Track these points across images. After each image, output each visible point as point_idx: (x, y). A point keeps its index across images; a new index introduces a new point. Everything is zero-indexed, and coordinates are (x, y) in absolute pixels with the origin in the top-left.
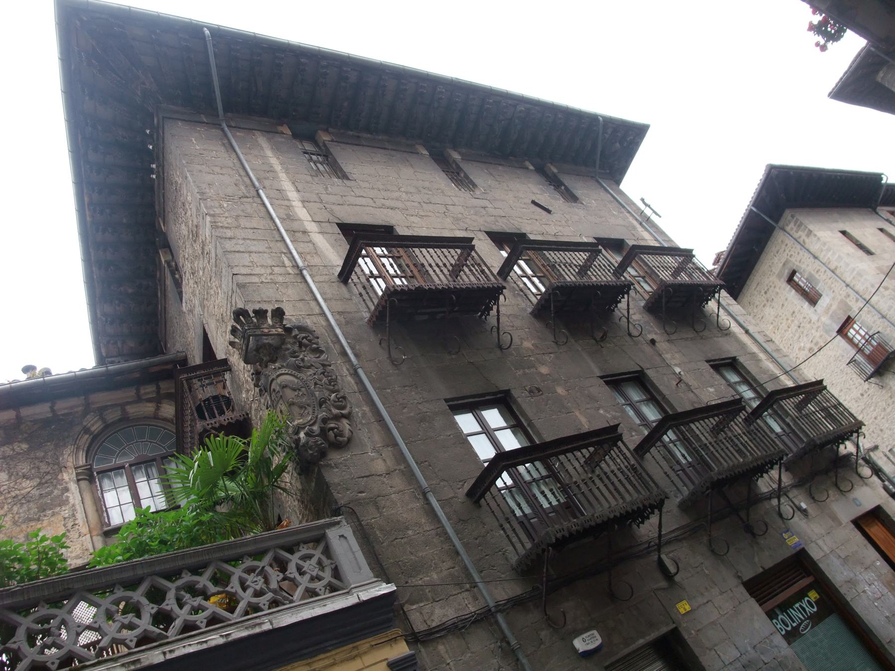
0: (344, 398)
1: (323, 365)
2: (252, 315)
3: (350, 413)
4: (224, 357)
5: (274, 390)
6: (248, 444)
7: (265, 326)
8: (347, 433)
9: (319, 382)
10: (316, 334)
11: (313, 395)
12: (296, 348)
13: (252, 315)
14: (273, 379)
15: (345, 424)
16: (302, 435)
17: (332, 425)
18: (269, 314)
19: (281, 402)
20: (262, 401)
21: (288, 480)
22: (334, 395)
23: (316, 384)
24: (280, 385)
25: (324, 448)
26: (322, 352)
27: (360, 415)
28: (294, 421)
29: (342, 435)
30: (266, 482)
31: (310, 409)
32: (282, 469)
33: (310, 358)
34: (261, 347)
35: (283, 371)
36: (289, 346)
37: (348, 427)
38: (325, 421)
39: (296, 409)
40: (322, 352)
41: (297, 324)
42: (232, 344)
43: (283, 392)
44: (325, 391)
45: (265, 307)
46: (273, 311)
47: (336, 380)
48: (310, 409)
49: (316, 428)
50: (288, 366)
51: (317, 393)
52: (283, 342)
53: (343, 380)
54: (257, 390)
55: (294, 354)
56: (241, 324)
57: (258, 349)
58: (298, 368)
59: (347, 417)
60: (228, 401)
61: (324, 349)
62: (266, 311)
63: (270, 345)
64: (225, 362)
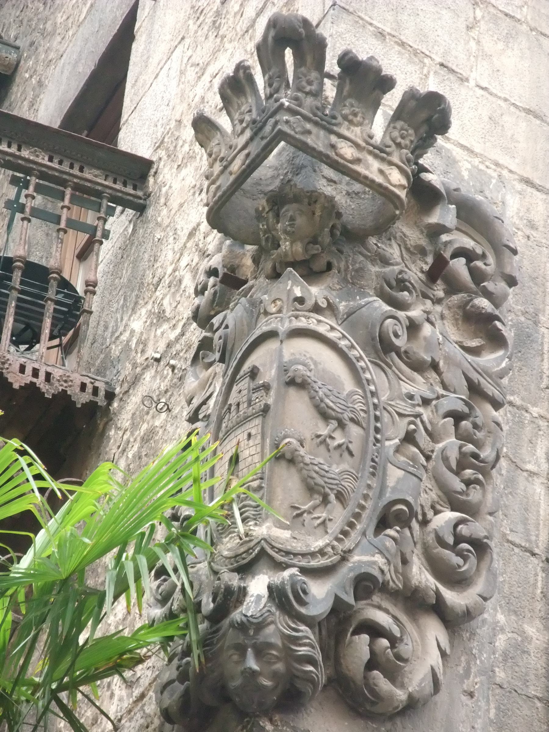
0: (480, 547)
1: (475, 389)
2: (332, 65)
3: (469, 615)
4: (144, 151)
5: (254, 373)
6: (54, 502)
7: (355, 133)
8: (417, 679)
9: (423, 438)
10: (514, 264)
11: (377, 470)
12: (415, 273)
13: (332, 65)
14: (272, 335)
15: (427, 643)
16: (258, 585)
17: (382, 618)
18: (391, 100)
19: (254, 427)
20: (191, 383)
21: (112, 710)
22: (449, 516)
23: (409, 438)
24: (284, 369)
25: (309, 679)
26: (497, 340)
27: (501, 641)
28: (258, 518)
29: (393, 675)
30: (37, 669)
31: (338, 515)
32: (119, 659)
33: (442, 334)
34: (296, 199)
35: (323, 325)
36: (394, 251)
37: (434, 658)
38: (366, 585)
39: (288, 486)
40: (497, 340)
41: (469, 190)
42: (203, 126)
43: (281, 398)
44: (427, 483)
45: (391, 63)
46: (411, 96)
47: (486, 469)
48: (338, 515)
49: (320, 594)
50: (349, 319)
51: (394, 474)
52: (382, 227)
53: (511, 482)
54: (196, 334)
55: (393, 291)
56: (277, 78)
57: (278, 200)
58: (382, 347)
59: (454, 622)
60: (71, 314)
61: (509, 333)
62: (386, 84)
63: (331, 209)
64: (138, 170)
